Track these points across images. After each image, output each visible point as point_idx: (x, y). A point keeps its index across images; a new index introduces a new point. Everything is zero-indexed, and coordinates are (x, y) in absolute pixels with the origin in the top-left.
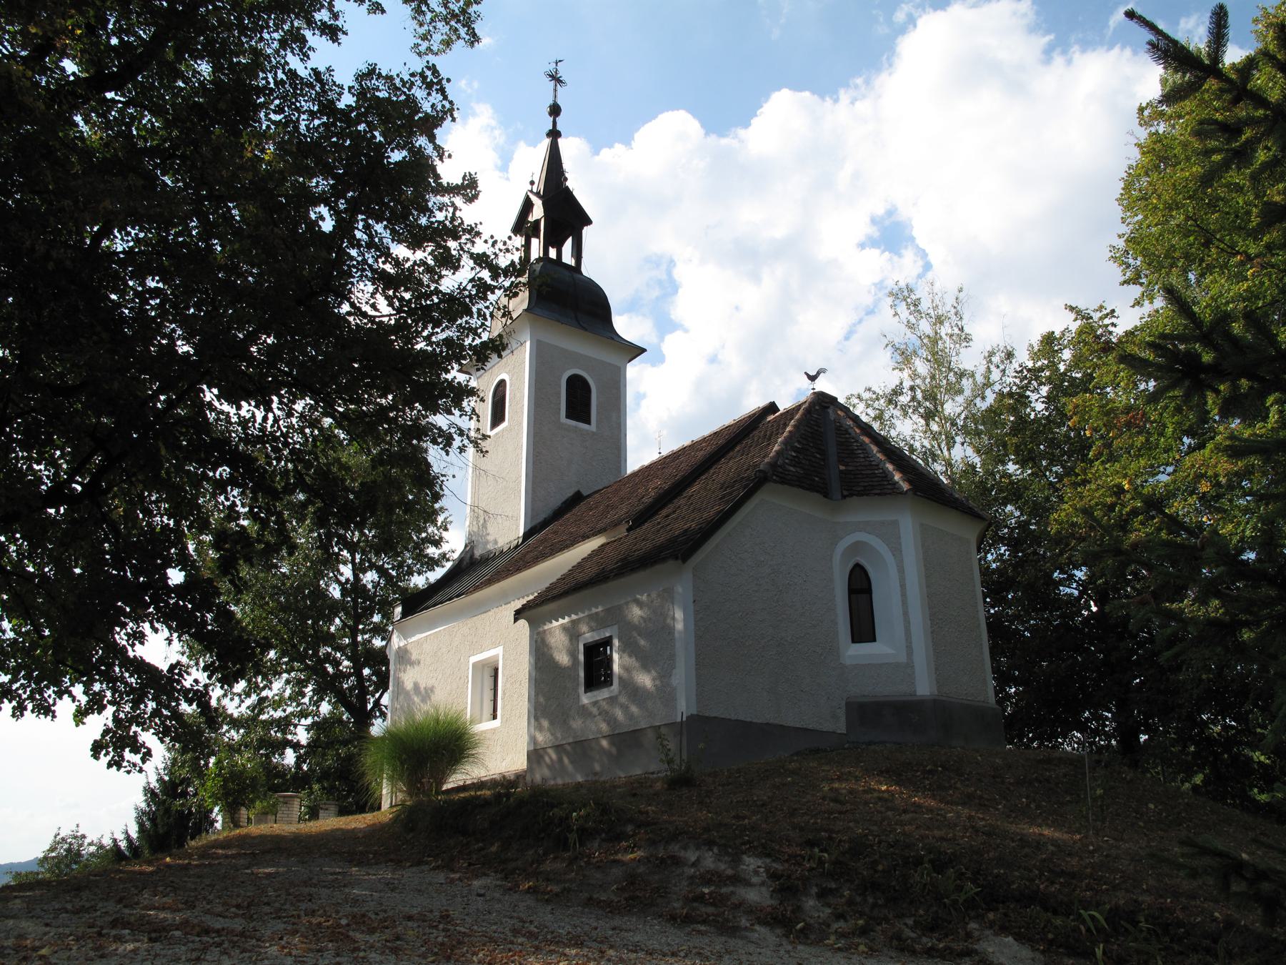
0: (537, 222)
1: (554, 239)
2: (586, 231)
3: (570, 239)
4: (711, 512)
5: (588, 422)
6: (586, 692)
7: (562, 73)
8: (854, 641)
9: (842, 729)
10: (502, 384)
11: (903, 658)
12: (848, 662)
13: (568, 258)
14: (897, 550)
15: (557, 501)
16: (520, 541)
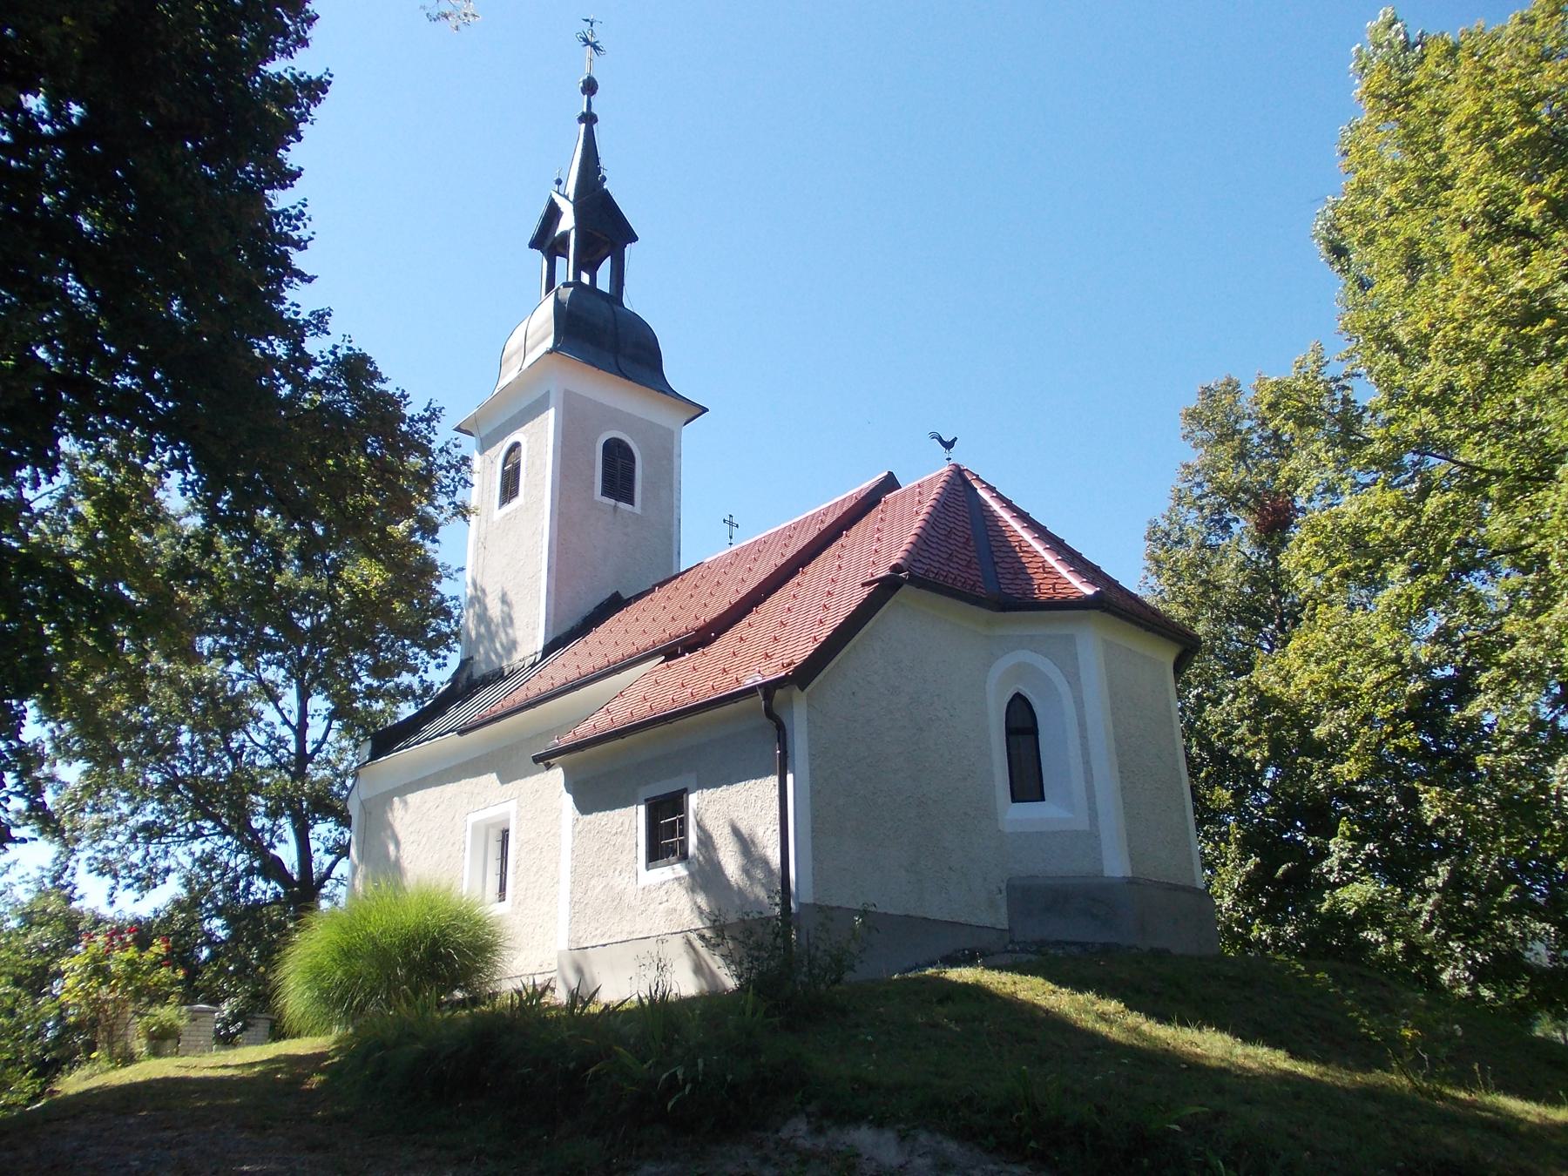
0: (566, 235)
1: (588, 262)
2: (630, 250)
3: (609, 259)
4: (498, 709)
5: (631, 501)
6: (648, 868)
7: (599, 37)
8: (1015, 799)
9: (1004, 923)
10: (516, 446)
11: (1083, 824)
12: (1007, 829)
13: (604, 283)
14: (1074, 679)
15: (588, 605)
16: (539, 657)
